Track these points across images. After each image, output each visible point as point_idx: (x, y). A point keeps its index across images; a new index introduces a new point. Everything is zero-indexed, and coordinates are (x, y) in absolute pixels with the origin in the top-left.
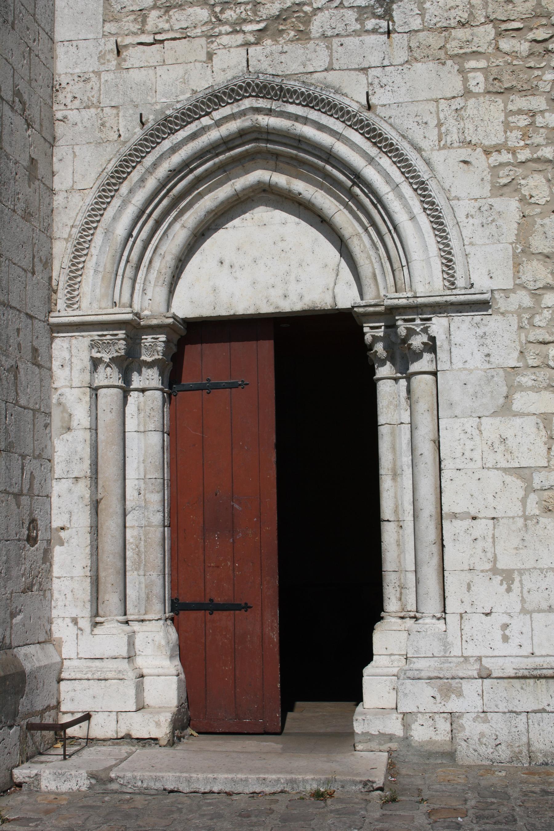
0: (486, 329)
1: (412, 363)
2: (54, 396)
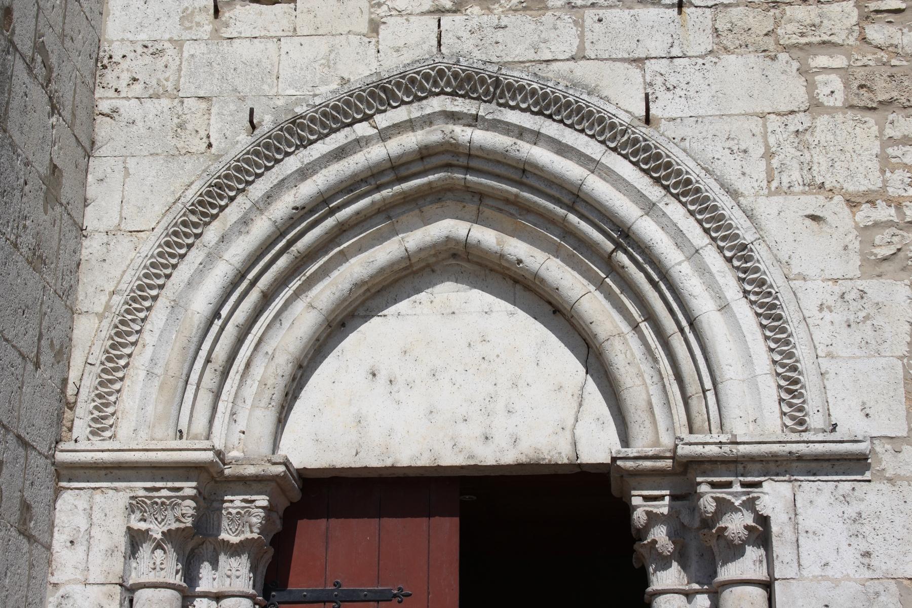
0: (862, 507)
1: (725, 563)
2: (51, 599)
